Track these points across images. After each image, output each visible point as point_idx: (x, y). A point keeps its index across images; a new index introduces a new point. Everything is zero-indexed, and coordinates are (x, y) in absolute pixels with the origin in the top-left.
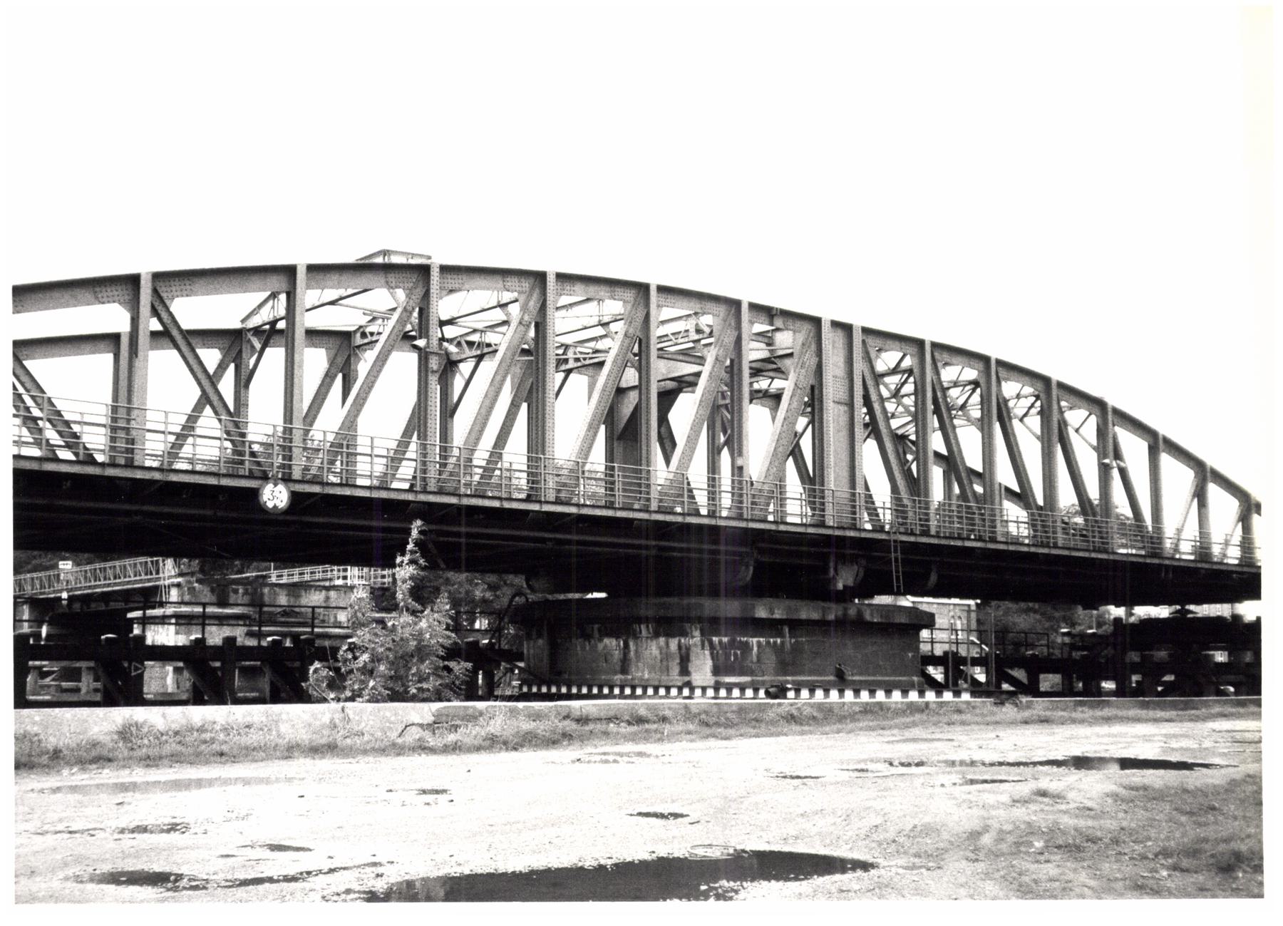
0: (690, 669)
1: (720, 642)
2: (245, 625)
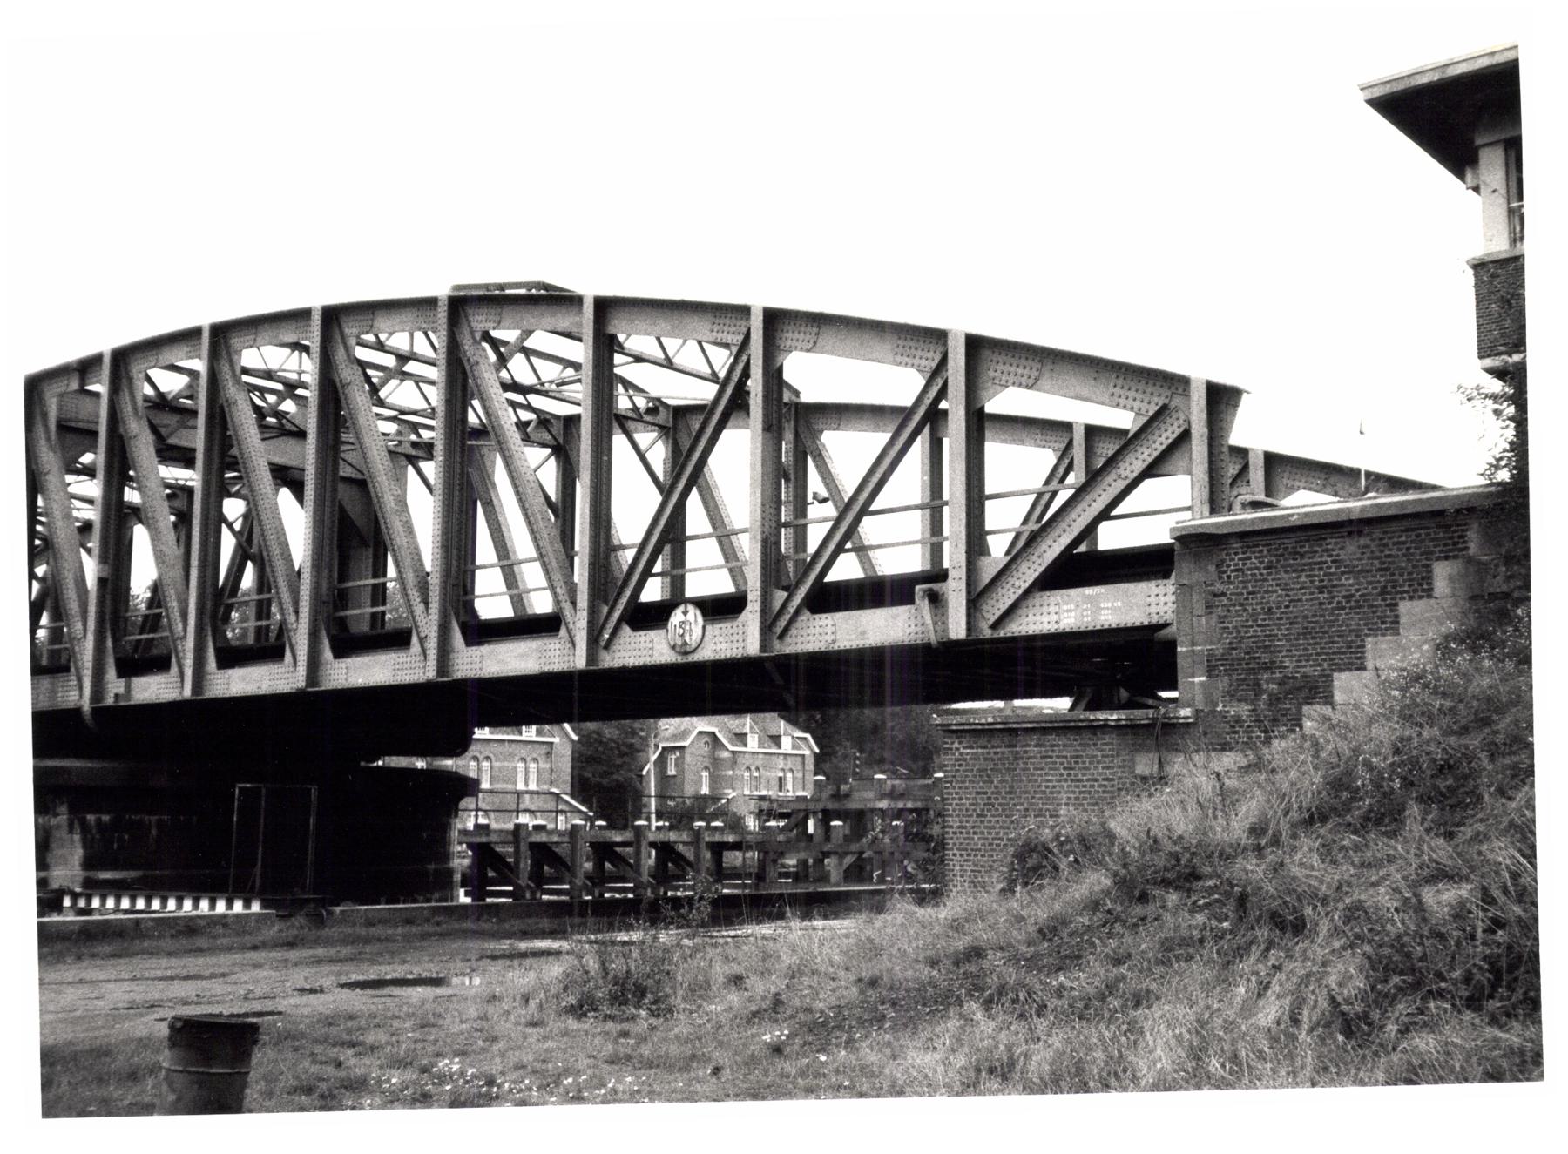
0: (48, 860)
1: (99, 821)
2: (1178, 718)
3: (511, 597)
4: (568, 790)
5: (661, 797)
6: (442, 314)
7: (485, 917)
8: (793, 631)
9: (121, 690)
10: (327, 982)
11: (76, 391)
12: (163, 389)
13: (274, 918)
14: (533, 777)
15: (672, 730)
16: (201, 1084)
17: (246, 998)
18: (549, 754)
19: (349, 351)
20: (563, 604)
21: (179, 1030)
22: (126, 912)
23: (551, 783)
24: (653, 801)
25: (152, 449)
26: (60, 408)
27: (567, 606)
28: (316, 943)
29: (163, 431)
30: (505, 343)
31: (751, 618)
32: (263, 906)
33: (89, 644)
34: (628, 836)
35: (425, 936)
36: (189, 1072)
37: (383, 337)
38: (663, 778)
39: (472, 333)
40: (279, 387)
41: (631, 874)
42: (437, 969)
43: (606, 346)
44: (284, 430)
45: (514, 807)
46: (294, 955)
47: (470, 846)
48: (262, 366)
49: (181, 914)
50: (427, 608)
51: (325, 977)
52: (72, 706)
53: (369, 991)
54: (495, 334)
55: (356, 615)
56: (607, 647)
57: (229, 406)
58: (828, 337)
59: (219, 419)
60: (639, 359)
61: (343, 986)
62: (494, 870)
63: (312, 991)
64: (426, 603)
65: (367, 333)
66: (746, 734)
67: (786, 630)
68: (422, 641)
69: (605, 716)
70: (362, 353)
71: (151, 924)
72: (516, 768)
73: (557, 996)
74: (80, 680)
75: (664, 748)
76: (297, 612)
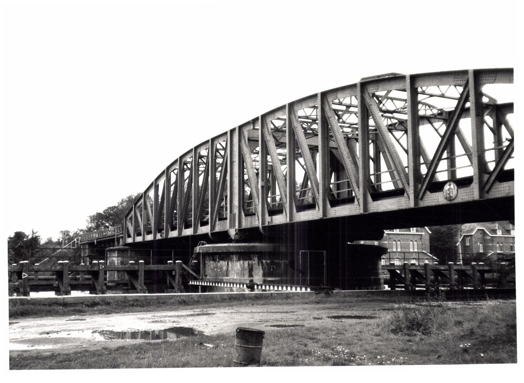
1: (266, 262)
3: (393, 182)
4: (429, 252)
5: (464, 253)
6: (358, 89)
7: (386, 295)
8: (492, 190)
9: (270, 220)
10: (324, 316)
11: (253, 129)
12: (277, 126)
13: (314, 294)
14: (416, 247)
15: (467, 229)
16: (246, 351)
17: (296, 320)
18: (421, 239)
19: (329, 106)
20: (405, 185)
21: (239, 332)
22: (276, 291)
23: (423, 249)
24: (461, 255)
25: (274, 144)
26: (249, 134)
27: (406, 185)
28: (325, 302)
29: (278, 138)
30: (381, 97)
31: (475, 187)
32: (311, 289)
33: (260, 206)
34: (446, 267)
35: (363, 301)
36: (242, 346)
37: (341, 100)
38: (465, 247)
39: (369, 94)
40: (311, 121)
41: (424, 281)
42: (362, 313)
43: (414, 93)
44: (310, 134)
45: (406, 258)
46: (318, 306)
47: (389, 270)
48: (304, 115)
49: (288, 292)
50: (359, 189)
51: (324, 314)
52: (257, 226)
53: (336, 320)
54: (377, 93)
55: (342, 192)
56: (421, 199)
57: (295, 128)
58: (498, 76)
59: (292, 133)
60: (431, 96)
61: (328, 317)
62: (417, 278)
63: (318, 319)
64: (359, 187)
65: (335, 99)
66: (496, 230)
67: (490, 189)
68: (358, 200)
69: (441, 224)
70: (334, 107)
71: (275, 295)
72: (409, 244)
73: (389, 326)
74: (258, 217)
75: (464, 236)
76: (318, 193)
